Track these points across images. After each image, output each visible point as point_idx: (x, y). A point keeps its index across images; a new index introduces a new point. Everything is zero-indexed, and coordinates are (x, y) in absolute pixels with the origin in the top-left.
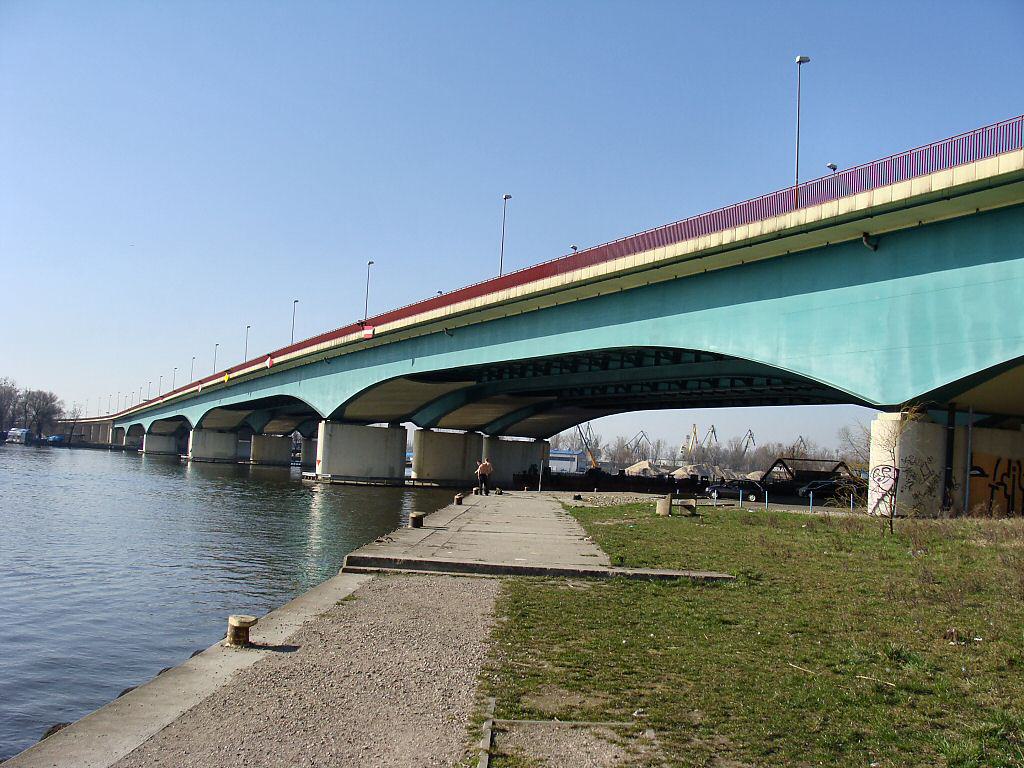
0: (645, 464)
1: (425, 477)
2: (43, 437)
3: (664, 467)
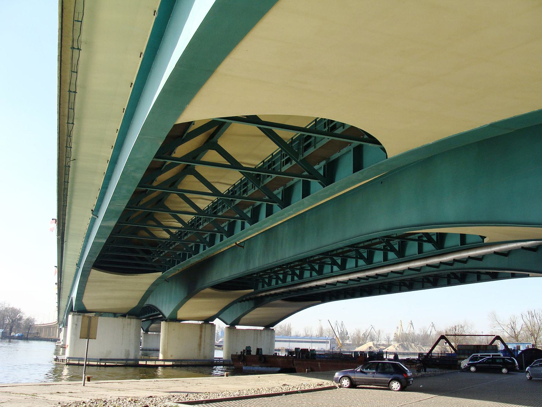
0: (370, 344)
1: (169, 358)
2: (13, 334)
3: (383, 345)
